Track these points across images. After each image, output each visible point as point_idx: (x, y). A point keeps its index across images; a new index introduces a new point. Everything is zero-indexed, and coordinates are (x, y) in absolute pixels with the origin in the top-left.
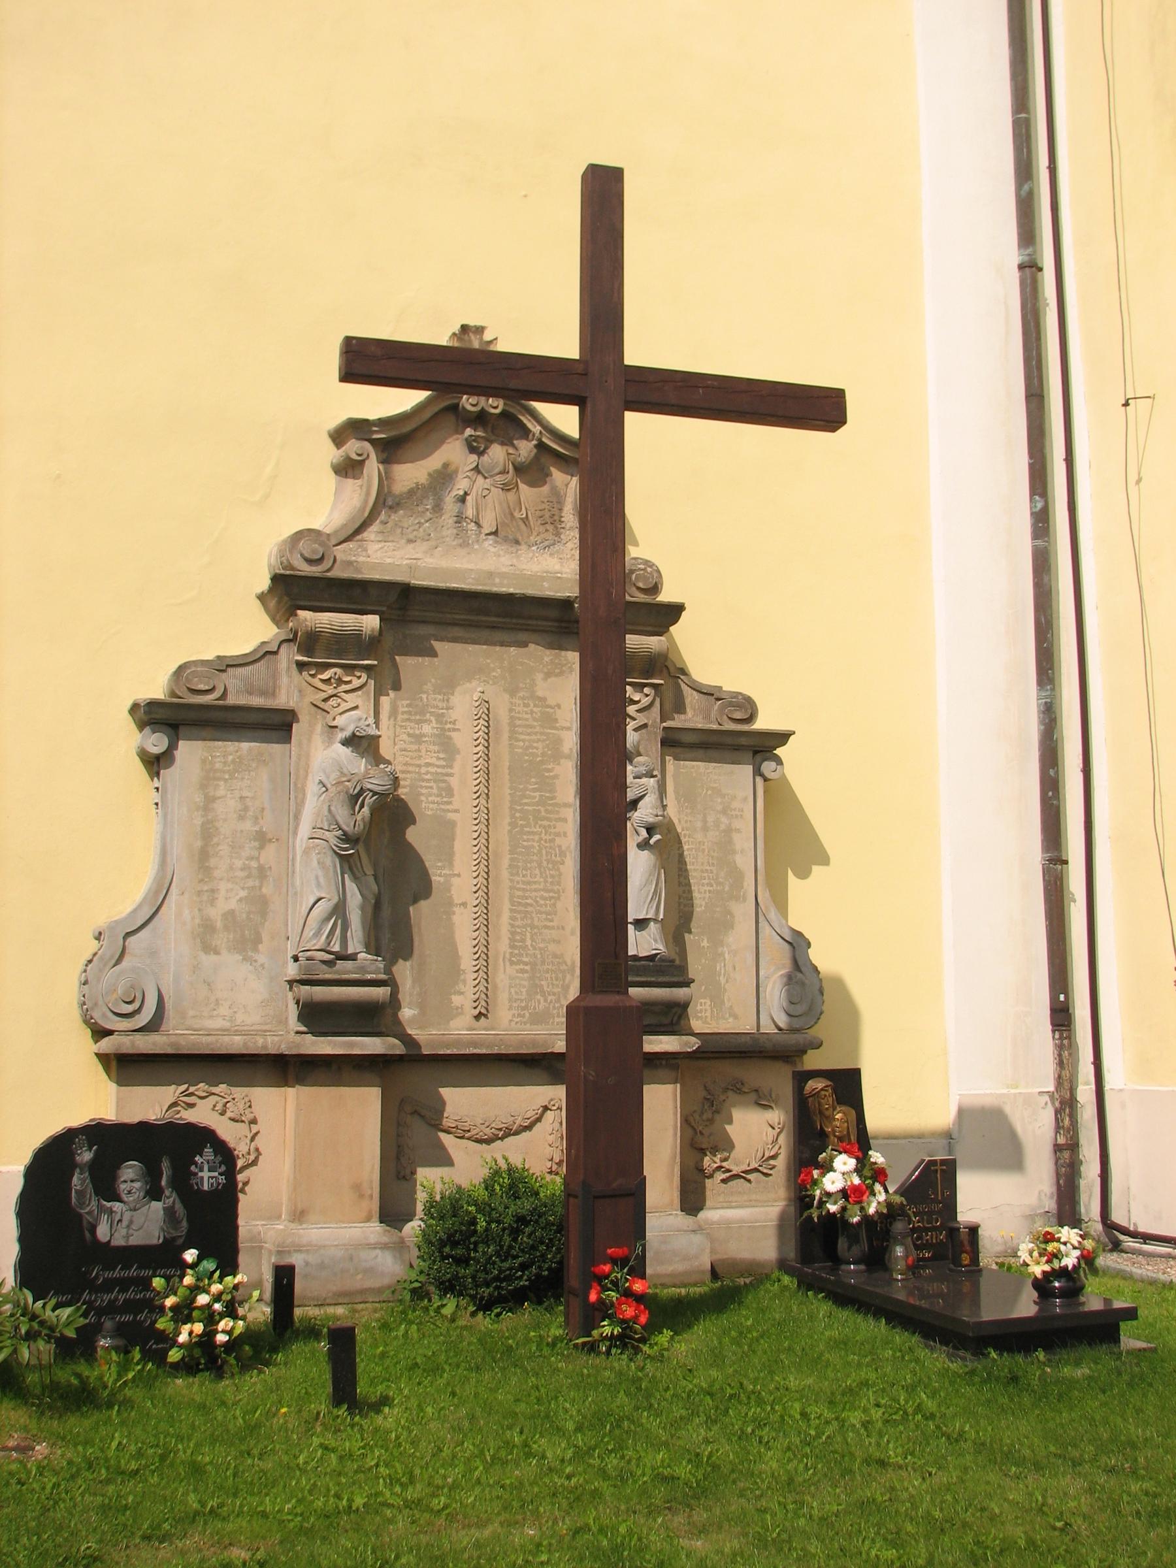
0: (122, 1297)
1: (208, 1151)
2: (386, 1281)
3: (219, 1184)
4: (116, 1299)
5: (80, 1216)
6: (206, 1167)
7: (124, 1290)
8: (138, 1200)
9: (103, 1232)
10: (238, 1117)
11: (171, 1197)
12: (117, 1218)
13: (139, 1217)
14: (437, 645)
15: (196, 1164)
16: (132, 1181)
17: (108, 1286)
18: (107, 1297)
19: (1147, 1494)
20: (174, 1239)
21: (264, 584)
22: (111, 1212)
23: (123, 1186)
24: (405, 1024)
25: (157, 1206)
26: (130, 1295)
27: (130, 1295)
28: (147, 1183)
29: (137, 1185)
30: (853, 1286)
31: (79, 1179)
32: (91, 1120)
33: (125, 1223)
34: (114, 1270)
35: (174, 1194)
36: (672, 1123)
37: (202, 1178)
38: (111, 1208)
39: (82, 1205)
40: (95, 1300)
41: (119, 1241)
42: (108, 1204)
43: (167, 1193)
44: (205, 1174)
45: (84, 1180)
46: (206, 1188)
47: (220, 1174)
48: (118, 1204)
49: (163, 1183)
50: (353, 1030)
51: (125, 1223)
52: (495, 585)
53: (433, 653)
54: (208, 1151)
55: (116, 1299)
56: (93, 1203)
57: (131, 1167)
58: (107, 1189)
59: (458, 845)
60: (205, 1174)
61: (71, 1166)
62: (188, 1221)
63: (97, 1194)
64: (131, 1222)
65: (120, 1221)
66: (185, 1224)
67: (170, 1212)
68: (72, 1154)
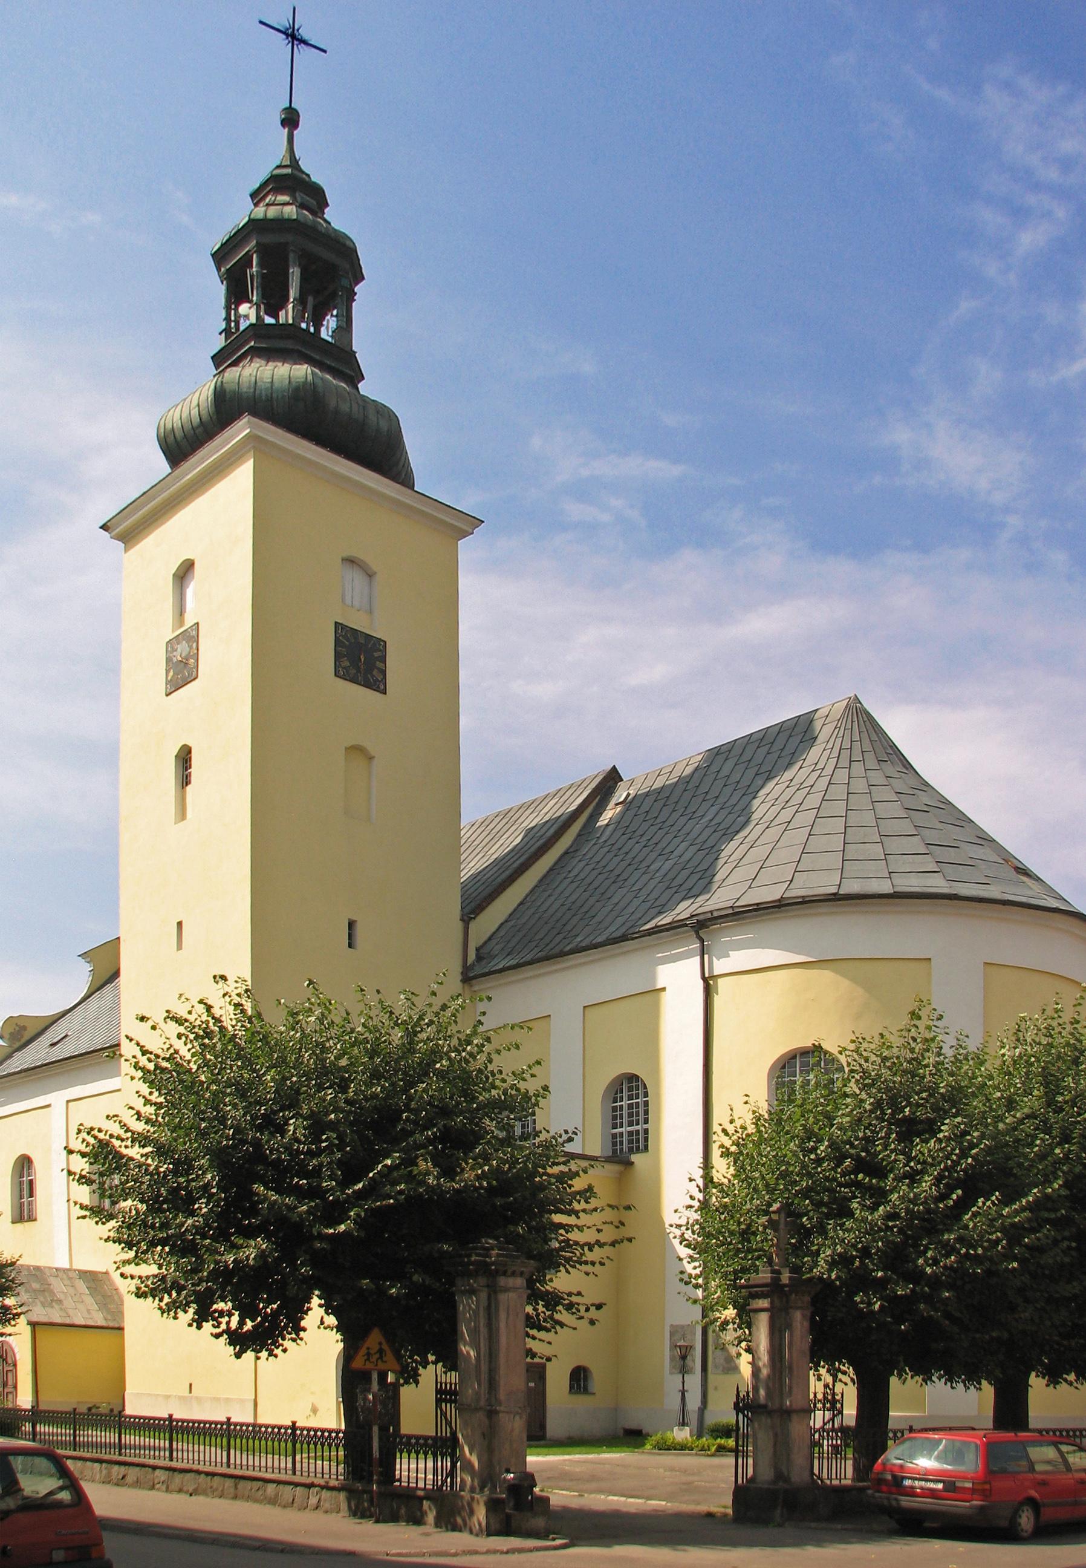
30: (514, 1478)
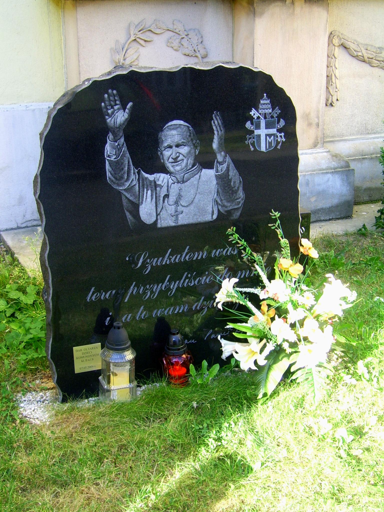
0: (174, 286)
1: (265, 102)
2: (335, 201)
3: (278, 143)
4: (168, 289)
5: (119, 193)
6: (263, 123)
7: (176, 278)
8: (187, 170)
9: (147, 212)
10: (192, 53)
11: (224, 162)
12: (163, 192)
13: (188, 190)
14: (266, 361)
15: (251, 118)
16: (178, 146)
17: (158, 275)
18: (157, 288)
19: (64, 498)
20: (229, 213)
21: (290, 328)
22: (155, 186)
23: (167, 153)
24: (67, 91)
25: (209, 174)
26: (184, 282)
27: (184, 282)
28: (196, 147)
29: (184, 150)
30: (192, 296)
31: (113, 147)
32: (35, 194)
33: (172, 199)
34: (180, 279)
35: (228, 159)
36: (148, 66)
37: (259, 136)
38: (174, 396)
39: (119, 179)
40: (144, 293)
41: (166, 221)
42: (151, 177)
43: (220, 158)
44: (262, 132)
45: (119, 149)
46: (263, 149)
47: (279, 131)
48: (163, 175)
49: (215, 145)
50: (327, 218)
51: (172, 199)
52: (50, 363)
53: (265, 359)
54: (265, 102)
55: (168, 289)
56: (132, 177)
57: (176, 127)
58: (147, 157)
59: (38, 187)
60: (262, 132)
61: (101, 132)
62: (244, 189)
63: (136, 166)
64: (180, 196)
65: (167, 196)
66: (241, 194)
67: (223, 180)
68: (101, 115)
